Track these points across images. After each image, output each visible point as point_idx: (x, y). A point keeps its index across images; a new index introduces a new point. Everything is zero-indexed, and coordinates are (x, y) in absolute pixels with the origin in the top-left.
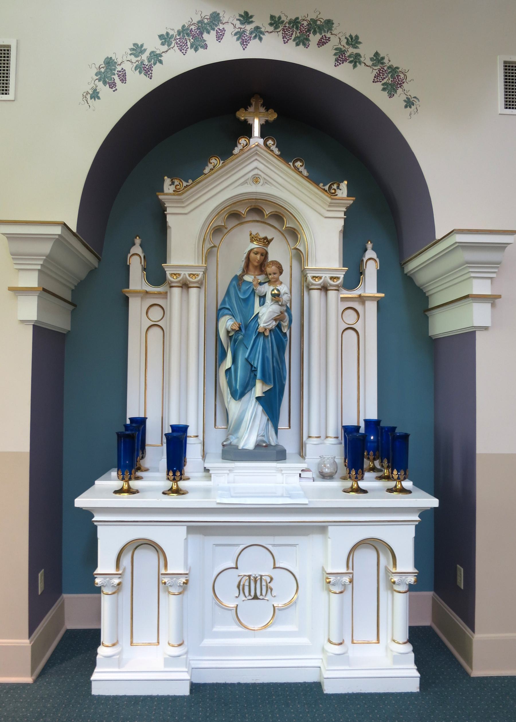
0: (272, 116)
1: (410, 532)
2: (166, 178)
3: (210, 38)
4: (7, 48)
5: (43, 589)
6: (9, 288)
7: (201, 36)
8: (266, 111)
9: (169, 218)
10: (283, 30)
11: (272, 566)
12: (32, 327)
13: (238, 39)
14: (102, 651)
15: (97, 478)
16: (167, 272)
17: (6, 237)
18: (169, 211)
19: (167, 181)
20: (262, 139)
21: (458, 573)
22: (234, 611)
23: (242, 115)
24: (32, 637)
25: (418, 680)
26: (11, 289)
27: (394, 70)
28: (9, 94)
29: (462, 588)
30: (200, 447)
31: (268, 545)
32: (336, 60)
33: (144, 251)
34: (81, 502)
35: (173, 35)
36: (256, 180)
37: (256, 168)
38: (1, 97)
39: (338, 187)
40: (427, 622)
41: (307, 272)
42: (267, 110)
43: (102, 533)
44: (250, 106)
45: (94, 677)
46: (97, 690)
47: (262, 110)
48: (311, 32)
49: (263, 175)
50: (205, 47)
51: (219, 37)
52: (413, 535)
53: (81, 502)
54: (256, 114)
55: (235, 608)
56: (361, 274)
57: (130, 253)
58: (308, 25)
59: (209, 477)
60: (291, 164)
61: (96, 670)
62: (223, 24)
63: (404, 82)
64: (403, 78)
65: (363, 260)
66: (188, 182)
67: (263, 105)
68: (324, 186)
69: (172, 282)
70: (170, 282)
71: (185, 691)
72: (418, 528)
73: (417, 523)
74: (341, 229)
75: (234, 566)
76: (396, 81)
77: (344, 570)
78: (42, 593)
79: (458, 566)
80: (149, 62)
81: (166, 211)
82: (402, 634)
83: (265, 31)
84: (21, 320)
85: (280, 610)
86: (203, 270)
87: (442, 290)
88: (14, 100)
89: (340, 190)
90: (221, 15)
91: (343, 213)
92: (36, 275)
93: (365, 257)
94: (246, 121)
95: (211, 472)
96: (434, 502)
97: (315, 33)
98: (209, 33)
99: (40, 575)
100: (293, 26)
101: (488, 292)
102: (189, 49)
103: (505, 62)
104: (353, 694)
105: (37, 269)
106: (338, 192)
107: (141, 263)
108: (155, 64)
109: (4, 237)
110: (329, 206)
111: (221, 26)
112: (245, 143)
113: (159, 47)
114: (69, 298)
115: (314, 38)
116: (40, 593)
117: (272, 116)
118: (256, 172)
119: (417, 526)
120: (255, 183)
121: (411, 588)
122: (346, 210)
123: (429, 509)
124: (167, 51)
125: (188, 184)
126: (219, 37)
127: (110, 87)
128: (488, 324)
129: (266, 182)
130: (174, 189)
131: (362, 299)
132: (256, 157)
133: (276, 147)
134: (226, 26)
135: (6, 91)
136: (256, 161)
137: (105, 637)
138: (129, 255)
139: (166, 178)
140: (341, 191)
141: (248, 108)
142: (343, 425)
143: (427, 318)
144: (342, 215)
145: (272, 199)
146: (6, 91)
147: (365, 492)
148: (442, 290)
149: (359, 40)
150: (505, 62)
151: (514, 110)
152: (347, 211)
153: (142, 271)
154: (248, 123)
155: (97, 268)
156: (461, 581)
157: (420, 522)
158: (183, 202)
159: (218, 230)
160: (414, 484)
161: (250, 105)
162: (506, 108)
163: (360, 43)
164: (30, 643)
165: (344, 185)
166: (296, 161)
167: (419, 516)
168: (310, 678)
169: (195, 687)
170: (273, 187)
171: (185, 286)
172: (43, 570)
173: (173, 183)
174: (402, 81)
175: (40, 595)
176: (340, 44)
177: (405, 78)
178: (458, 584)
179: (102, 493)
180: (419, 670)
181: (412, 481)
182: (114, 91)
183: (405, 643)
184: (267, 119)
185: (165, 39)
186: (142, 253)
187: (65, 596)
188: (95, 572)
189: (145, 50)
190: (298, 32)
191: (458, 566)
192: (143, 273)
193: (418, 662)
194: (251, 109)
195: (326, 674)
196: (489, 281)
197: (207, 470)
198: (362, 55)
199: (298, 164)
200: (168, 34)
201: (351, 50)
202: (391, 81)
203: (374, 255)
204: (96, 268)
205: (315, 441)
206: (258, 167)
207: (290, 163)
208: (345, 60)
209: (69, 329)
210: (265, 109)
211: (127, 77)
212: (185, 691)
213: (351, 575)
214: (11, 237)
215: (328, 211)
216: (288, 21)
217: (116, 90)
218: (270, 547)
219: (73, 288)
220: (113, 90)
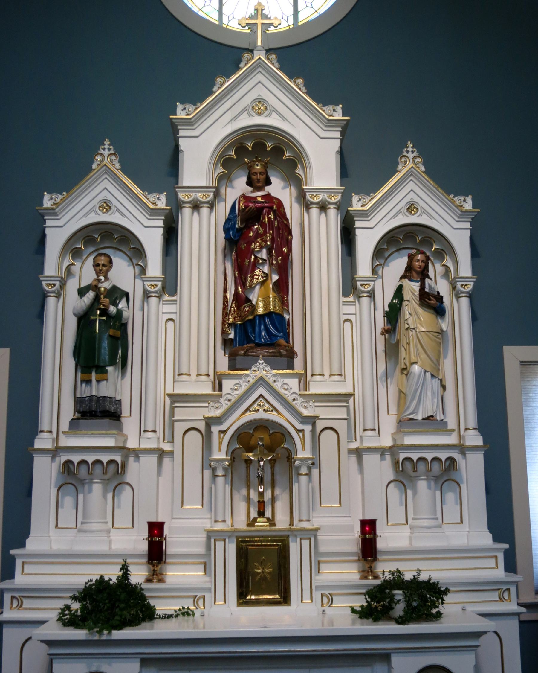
140: (338, 113)
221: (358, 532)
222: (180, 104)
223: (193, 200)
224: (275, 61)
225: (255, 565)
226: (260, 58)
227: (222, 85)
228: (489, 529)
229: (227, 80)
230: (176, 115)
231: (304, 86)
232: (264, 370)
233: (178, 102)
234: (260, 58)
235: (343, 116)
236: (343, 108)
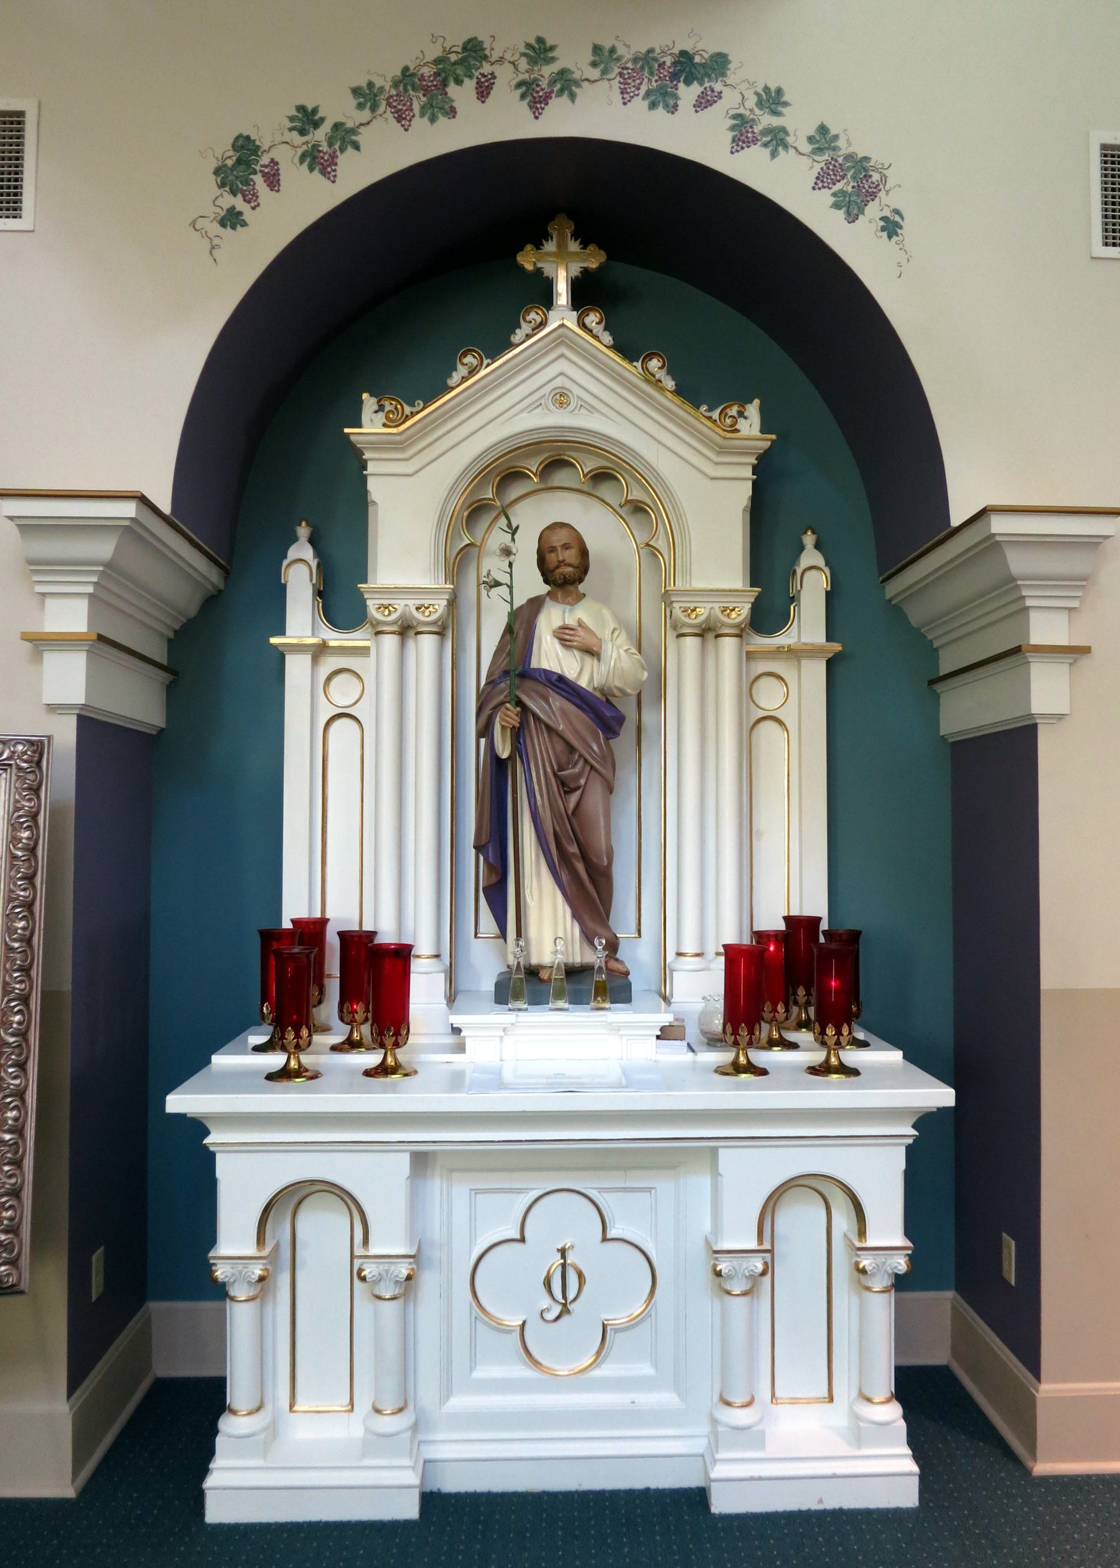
0: (594, 260)
1: (896, 1161)
2: (365, 396)
3: (462, 94)
4: (17, 117)
5: (101, 1289)
6: (23, 633)
7: (444, 90)
8: (581, 249)
9: (372, 485)
10: (621, 75)
11: (600, 1236)
12: (74, 719)
13: (523, 97)
14: (230, 1426)
15: (215, 1049)
16: (369, 603)
17: (18, 525)
18: (371, 468)
19: (369, 402)
20: (575, 312)
21: (1005, 1252)
22: (517, 1335)
23: (527, 260)
24: (73, 1399)
25: (915, 1482)
26: (26, 637)
27: (861, 166)
28: (21, 217)
29: (1013, 1283)
30: (440, 980)
31: (590, 1190)
32: (734, 141)
33: (318, 553)
34: (177, 1102)
35: (382, 89)
36: (561, 398)
37: (562, 374)
38: (5, 224)
39: (741, 414)
40: (938, 1355)
41: (673, 599)
42: (585, 245)
43: (225, 1168)
44: (547, 240)
45: (210, 1482)
46: (217, 1512)
47: (574, 246)
48: (682, 79)
49: (577, 391)
50: (452, 112)
51: (484, 91)
52: (902, 1165)
53: (177, 1102)
54: (562, 254)
55: (518, 1328)
56: (793, 599)
57: (285, 557)
58: (674, 64)
59: (460, 1048)
60: (639, 364)
61: (217, 1463)
62: (492, 64)
63: (880, 190)
64: (878, 181)
65: (795, 572)
66: (413, 406)
67: (575, 236)
68: (710, 410)
69: (379, 623)
70: (374, 623)
71: (410, 1510)
72: (912, 1152)
73: (910, 1141)
74: (745, 505)
75: (518, 1236)
76: (864, 188)
77: (753, 1245)
78: (97, 1299)
79: (1005, 1235)
80: (330, 145)
81: (366, 470)
82: (883, 1381)
83: (583, 78)
84: (49, 705)
85: (616, 1331)
86: (447, 597)
87: (969, 634)
88: (33, 231)
89: (746, 418)
90: (486, 45)
91: (750, 469)
92: (83, 605)
93: (799, 565)
94: (539, 272)
95: (463, 1034)
96: (943, 1096)
97: (688, 83)
98: (459, 82)
99: (94, 1258)
100: (642, 68)
101: (1063, 641)
102: (417, 118)
103: (1104, 147)
104: (800, 1513)
105: (86, 594)
106: (742, 424)
107: (311, 580)
108: (342, 150)
109: (11, 526)
110: (719, 453)
111: (486, 68)
112: (539, 320)
113: (353, 116)
114: (160, 656)
115: (688, 93)
116: (94, 1297)
117: (594, 260)
118: (559, 383)
119: (909, 1149)
120: (557, 405)
121: (900, 1283)
122: (756, 462)
123: (935, 1110)
124: (368, 123)
125: (415, 410)
126: (484, 91)
127: (245, 200)
128: (1064, 709)
129: (583, 405)
130: (384, 420)
131: (794, 654)
132: (563, 350)
133: (605, 329)
134: (497, 69)
135: (13, 209)
136: (561, 360)
137: (239, 1393)
138: (285, 563)
139: (365, 396)
140: (749, 421)
141: (543, 245)
142: (755, 929)
143: (937, 697)
144: (748, 472)
145: (590, 440)
146: (13, 209)
147: (763, 1072)
148: (969, 634)
149: (785, 99)
150: (1104, 147)
151: (1118, 249)
152: (758, 464)
153: (314, 599)
154: (545, 275)
155: (222, 590)
156: (1010, 1266)
157: (917, 1140)
158: (403, 450)
159: (476, 511)
160: (905, 1057)
161: (547, 237)
162: (1106, 244)
163: (786, 104)
164: (71, 1409)
165: (753, 410)
166: (650, 357)
167: (915, 1126)
168: (689, 1480)
169: (430, 1500)
170: (596, 415)
171: (406, 630)
172: (102, 1249)
173: (381, 408)
174: (875, 188)
175: (95, 1302)
176: (742, 107)
177: (883, 181)
178: (1005, 1274)
179: (237, 1081)
180: (917, 1457)
181: (902, 1050)
182: (253, 208)
183: (888, 1401)
184: (585, 265)
185: (367, 96)
186: (314, 557)
187: (154, 1306)
188: (211, 1254)
189: (322, 119)
190: (653, 80)
191: (1005, 1235)
192: (316, 602)
193: (914, 1441)
194: (550, 246)
195: (719, 1471)
196: (1064, 617)
197: (456, 1031)
198: (790, 130)
199: (654, 364)
200: (370, 84)
201: (766, 120)
202: (853, 187)
203: (818, 559)
204: (220, 591)
205: (690, 963)
206: (564, 372)
207: (635, 364)
208: (547, 97)
209: (163, 725)
210: (581, 244)
211: (283, 177)
212: (410, 1510)
213: (768, 1255)
214: (28, 527)
215: (717, 464)
216: (631, 57)
217: (258, 205)
218: (593, 1194)
219: (171, 635)
220: (253, 205)
221: (820, 1501)
222: (371, 396)
223: (401, 617)
224: (598, 329)
225: (795, 993)
226: (562, 326)
227: (472, 372)
228: (908, 1443)
229: (486, 362)
230: (360, 426)
231: (669, 373)
232: (382, 402)
233: (366, 392)
234: (562, 326)
235: (751, 586)
236: (762, 410)
